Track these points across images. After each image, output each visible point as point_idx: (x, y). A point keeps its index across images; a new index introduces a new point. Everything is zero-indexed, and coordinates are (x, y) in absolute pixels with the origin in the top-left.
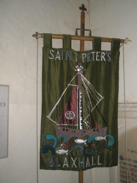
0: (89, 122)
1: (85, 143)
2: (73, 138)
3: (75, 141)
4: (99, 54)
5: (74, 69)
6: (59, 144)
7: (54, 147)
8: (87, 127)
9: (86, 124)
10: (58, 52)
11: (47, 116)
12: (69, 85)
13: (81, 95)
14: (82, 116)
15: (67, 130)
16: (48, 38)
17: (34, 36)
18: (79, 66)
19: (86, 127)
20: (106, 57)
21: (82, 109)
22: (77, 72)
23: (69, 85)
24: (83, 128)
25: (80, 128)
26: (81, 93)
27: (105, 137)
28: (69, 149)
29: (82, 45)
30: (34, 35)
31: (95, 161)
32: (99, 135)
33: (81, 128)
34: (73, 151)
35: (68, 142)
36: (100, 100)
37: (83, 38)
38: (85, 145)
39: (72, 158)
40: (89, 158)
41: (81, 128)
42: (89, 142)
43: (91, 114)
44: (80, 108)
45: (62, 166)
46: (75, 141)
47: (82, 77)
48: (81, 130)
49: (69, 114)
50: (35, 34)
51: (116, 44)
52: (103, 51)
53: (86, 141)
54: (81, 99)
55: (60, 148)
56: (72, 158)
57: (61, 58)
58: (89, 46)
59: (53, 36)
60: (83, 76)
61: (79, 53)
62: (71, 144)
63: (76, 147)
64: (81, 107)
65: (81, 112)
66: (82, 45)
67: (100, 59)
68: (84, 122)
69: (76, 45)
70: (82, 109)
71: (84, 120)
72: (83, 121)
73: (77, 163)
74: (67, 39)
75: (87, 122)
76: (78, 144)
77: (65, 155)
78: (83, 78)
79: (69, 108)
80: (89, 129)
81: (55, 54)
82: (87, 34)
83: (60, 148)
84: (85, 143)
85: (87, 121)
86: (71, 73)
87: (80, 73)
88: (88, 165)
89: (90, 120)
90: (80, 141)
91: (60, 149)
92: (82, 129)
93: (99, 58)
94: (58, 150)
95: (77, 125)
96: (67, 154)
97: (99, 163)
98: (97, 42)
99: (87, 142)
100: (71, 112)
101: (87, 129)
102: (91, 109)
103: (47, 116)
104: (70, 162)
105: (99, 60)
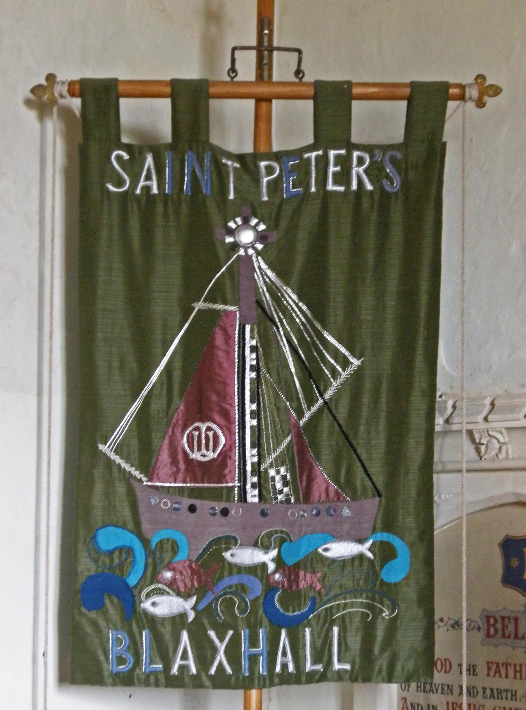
0: (292, 469)
1: (272, 567)
2: (216, 541)
3: (227, 555)
4: (344, 162)
5: (218, 231)
6: (152, 575)
7: (132, 580)
8: (281, 492)
9: (273, 479)
10: (149, 160)
11: (101, 447)
12: (199, 305)
13: (253, 349)
14: (257, 444)
15: (192, 509)
16: (100, 98)
17: (496, 91)
18: (246, 221)
19: (275, 493)
20: (375, 172)
21: (256, 414)
22: (235, 246)
23: (199, 305)
24: (261, 496)
25: (249, 499)
26: (254, 343)
27: (368, 544)
28: (201, 593)
29: (262, 121)
30: (40, 86)
31: (321, 654)
32: (339, 537)
33: (253, 496)
34: (216, 599)
35: (197, 561)
36: (344, 375)
37: (264, 90)
38: (269, 571)
39: (212, 634)
40: (289, 634)
41: (253, 496)
42: (290, 561)
43: (299, 436)
44: (250, 407)
45: (168, 667)
46: (227, 555)
47: (260, 268)
48: (255, 504)
49: (200, 436)
50: (45, 83)
51: (427, 103)
52: (358, 147)
53: (274, 553)
54: (253, 368)
55: (160, 586)
56: (212, 634)
57: (160, 186)
58: (294, 124)
59: (356, 91)
60: (264, 266)
61: (247, 163)
62: (208, 571)
63: (227, 581)
64: (252, 401)
65: (252, 427)
66: (262, 121)
67: (348, 184)
68: (266, 470)
69: (233, 126)
70: (256, 414)
71: (269, 460)
72: (263, 467)
73: (233, 653)
74: (191, 100)
75: (278, 472)
76: (240, 569)
77: (178, 621)
78: (263, 274)
79: (199, 411)
80: (288, 501)
81: (133, 166)
82: (282, 68)
83: (160, 586)
84: (272, 567)
85: (282, 465)
86: (203, 253)
87: (251, 251)
88: (284, 666)
89: (263, 400)
90: (246, 556)
91: (160, 592)
92: (256, 500)
93: (343, 177)
94: (148, 596)
95: (237, 484)
96: (191, 616)
97: (339, 661)
98: (332, 102)
99: (279, 560)
100: (209, 429)
101: (281, 502)
102: (300, 414)
103: (101, 447)
104: (204, 652)
105: (342, 189)
